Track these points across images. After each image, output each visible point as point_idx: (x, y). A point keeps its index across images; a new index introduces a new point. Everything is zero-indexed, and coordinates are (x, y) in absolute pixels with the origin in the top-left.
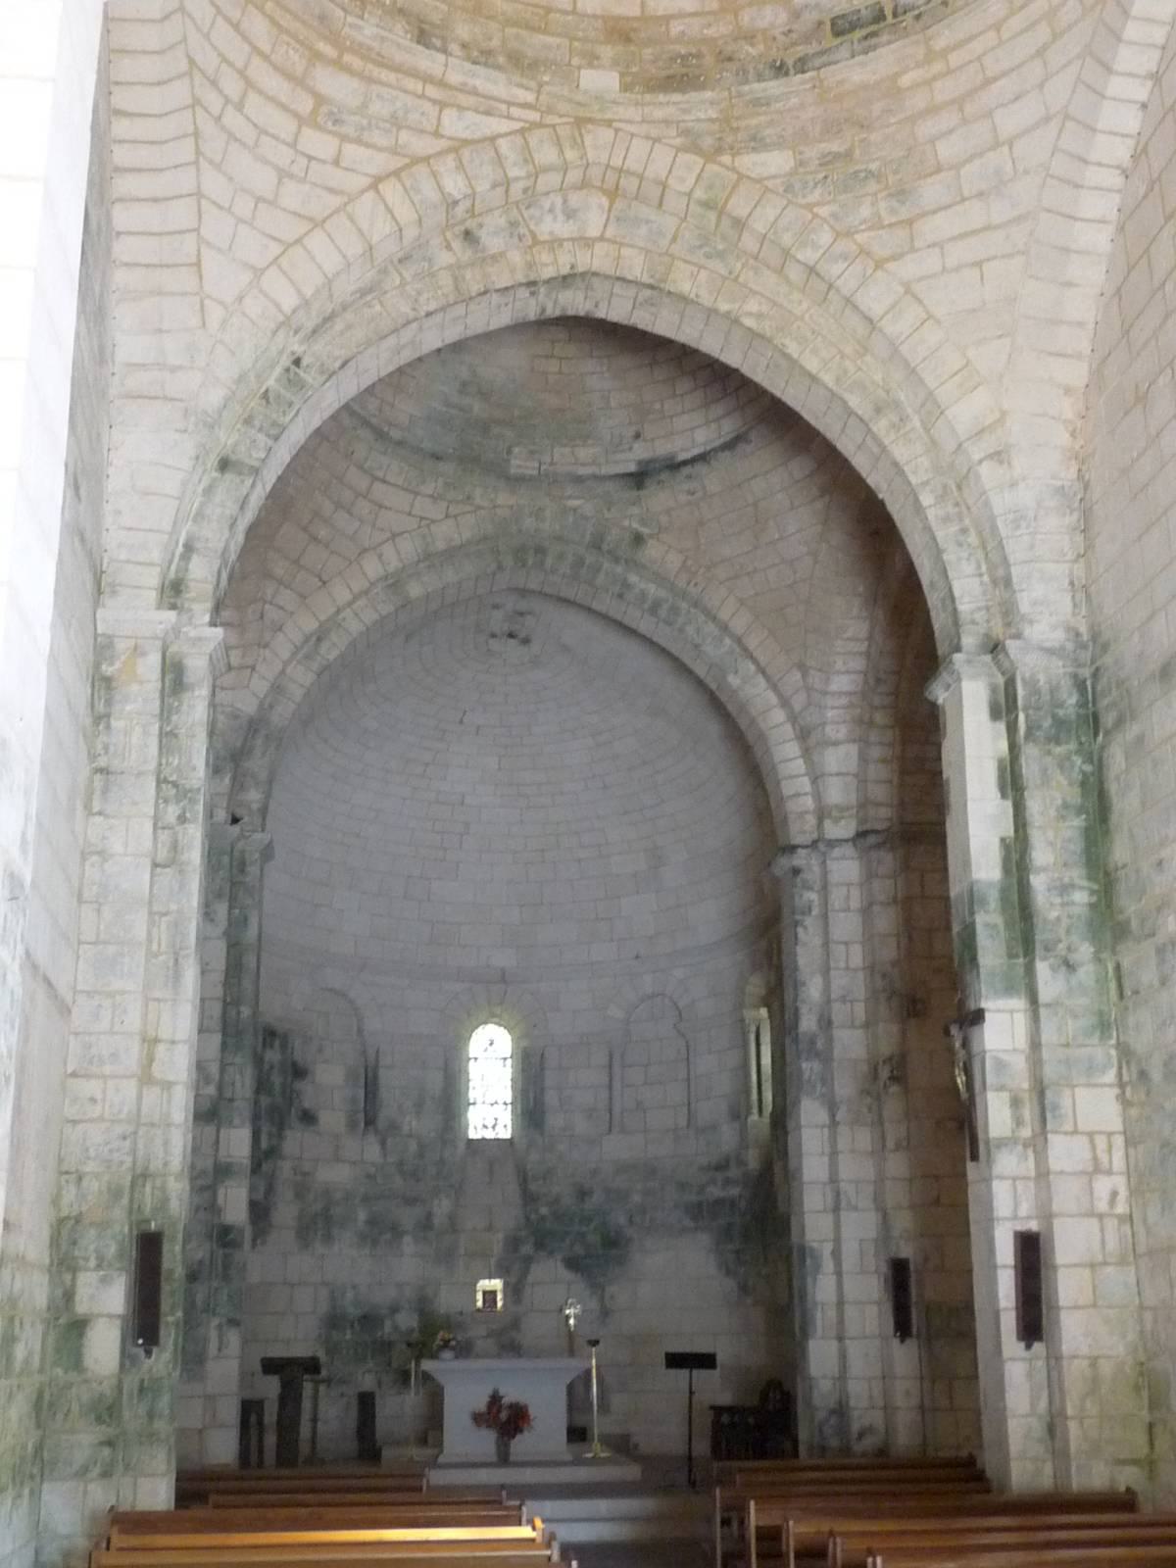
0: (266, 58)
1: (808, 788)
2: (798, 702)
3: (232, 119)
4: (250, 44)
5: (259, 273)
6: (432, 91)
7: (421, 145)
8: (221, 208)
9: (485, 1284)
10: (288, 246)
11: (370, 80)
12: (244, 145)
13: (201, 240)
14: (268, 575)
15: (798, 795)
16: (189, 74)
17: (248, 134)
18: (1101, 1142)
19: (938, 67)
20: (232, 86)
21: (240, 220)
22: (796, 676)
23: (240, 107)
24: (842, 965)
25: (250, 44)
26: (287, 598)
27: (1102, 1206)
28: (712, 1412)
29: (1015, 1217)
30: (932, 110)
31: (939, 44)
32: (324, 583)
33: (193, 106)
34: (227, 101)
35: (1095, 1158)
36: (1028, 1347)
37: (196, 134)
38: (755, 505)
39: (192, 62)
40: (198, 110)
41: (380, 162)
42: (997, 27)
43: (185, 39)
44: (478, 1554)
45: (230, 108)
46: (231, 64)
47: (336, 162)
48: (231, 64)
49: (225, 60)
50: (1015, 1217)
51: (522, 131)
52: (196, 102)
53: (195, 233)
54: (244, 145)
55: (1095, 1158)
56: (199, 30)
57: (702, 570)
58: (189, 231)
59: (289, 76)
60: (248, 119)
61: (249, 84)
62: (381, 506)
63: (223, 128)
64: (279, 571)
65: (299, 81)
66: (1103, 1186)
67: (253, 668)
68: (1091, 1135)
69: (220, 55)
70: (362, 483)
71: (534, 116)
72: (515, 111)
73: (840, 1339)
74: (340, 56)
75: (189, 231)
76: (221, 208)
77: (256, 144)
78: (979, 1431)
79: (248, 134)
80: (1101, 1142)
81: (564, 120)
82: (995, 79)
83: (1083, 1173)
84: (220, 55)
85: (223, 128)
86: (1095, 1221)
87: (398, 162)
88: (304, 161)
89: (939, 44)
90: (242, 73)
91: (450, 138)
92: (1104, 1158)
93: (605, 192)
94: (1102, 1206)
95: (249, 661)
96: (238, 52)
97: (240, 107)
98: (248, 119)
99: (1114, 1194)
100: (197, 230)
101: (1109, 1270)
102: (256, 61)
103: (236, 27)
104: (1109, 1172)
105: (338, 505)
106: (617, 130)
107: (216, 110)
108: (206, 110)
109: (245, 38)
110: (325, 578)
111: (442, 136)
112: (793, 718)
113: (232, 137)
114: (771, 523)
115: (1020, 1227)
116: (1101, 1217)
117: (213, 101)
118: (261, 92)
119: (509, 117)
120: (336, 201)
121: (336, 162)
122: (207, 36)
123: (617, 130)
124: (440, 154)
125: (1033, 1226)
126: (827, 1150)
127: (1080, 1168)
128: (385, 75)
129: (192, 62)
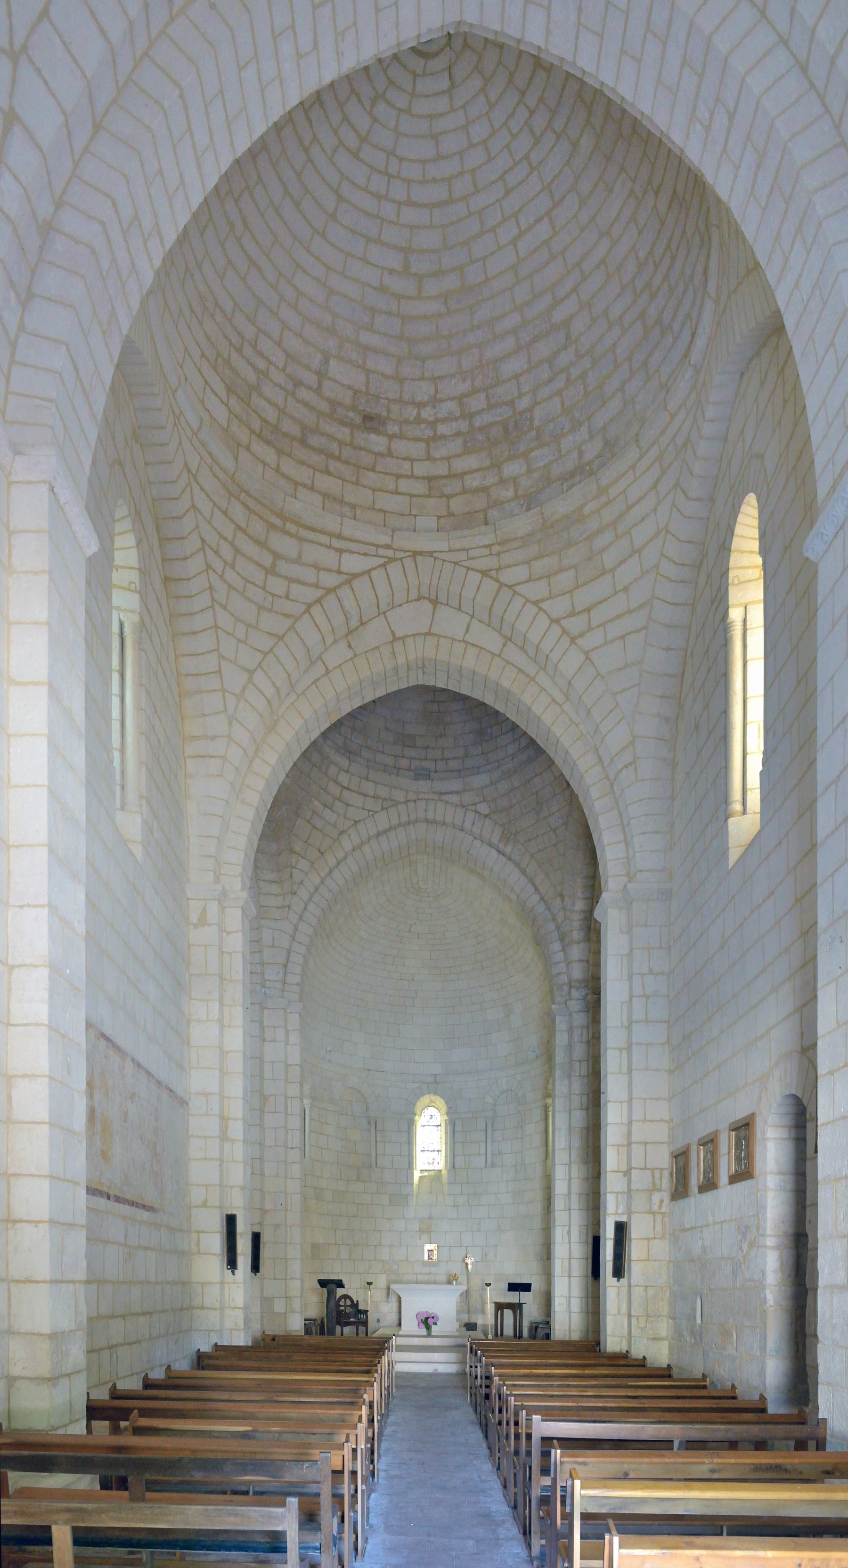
0: (244, 532)
1: (565, 970)
2: (560, 917)
3: (230, 574)
4: (235, 523)
5: (251, 673)
6: (336, 543)
7: (330, 580)
8: (228, 634)
9: (428, 1247)
10: (265, 654)
11: (301, 540)
12: (237, 591)
13: (220, 656)
14: (292, 851)
15: (559, 974)
16: (203, 549)
17: (239, 583)
18: (657, 1174)
19: (603, 499)
20: (227, 553)
21: (239, 640)
22: (558, 901)
23: (233, 567)
24: (577, 1074)
25: (235, 523)
26: (303, 864)
27: (655, 1208)
28: (313, 1305)
29: (617, 1213)
30: (600, 531)
31: (604, 482)
32: (322, 854)
33: (207, 570)
34: (226, 563)
35: (654, 1183)
36: (618, 1280)
37: (211, 588)
38: (537, 794)
39: (203, 541)
40: (210, 571)
41: (312, 594)
42: (633, 467)
43: (197, 527)
44: (565, 1404)
45: (228, 568)
46: (225, 539)
47: (287, 597)
48: (225, 539)
49: (221, 536)
50: (617, 1213)
51: (384, 565)
52: (209, 567)
53: (216, 652)
54: (237, 591)
55: (654, 1183)
56: (205, 518)
57: (512, 837)
58: (209, 652)
59: (258, 542)
60: (239, 574)
61: (237, 551)
62: (347, 805)
63: (225, 582)
64: (297, 849)
65: (262, 544)
66: (656, 1197)
67: (289, 907)
68: (653, 1170)
69: (219, 533)
70: (337, 791)
71: (390, 553)
72: (382, 552)
73: (569, 1277)
74: (284, 524)
75: (209, 652)
76: (228, 634)
77: (244, 591)
78: (261, 1304)
79: (239, 583)
80: (657, 1174)
81: (408, 554)
82: (633, 505)
83: (648, 1190)
84: (219, 533)
85: (225, 582)
86: (651, 1216)
87: (319, 593)
88: (270, 598)
89: (604, 482)
90: (232, 544)
91: (346, 574)
92: (657, 1181)
93: (431, 601)
94: (655, 1208)
95: (287, 903)
96: (228, 530)
97: (233, 567)
98: (239, 574)
99: (662, 1201)
100: (217, 650)
101: (657, 1241)
102: (239, 534)
103: (225, 513)
104: (660, 1190)
105: (325, 806)
106: (435, 558)
107: (220, 570)
108: (214, 571)
109: (232, 520)
110: (322, 851)
111: (343, 573)
112: (558, 928)
113: (231, 587)
114: (544, 805)
115: (618, 1219)
116: (654, 1213)
117: (217, 564)
118: (244, 555)
119: (378, 556)
120: (289, 622)
121: (287, 597)
122: (209, 522)
123: (435, 558)
124: (340, 586)
125: (624, 1219)
126: (567, 1177)
127: (646, 1188)
128: (311, 535)
129: (203, 541)
